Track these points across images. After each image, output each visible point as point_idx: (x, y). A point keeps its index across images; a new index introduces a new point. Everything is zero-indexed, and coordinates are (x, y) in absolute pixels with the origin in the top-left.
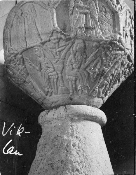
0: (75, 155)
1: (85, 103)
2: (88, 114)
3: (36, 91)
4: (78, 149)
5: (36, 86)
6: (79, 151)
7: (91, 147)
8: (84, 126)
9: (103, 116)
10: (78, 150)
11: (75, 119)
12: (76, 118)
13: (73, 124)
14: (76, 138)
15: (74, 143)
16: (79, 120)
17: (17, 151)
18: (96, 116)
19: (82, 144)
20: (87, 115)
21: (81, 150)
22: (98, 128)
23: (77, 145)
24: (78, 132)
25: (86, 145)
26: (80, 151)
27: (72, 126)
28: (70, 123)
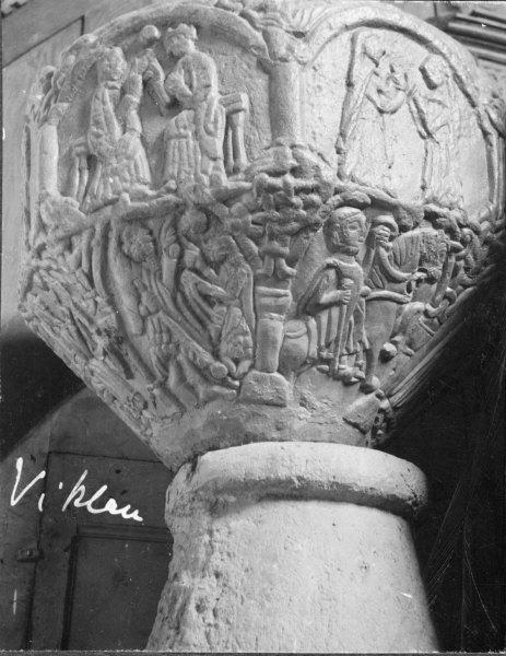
0: (195, 645)
1: (326, 436)
2: (259, 474)
3: (69, 309)
4: (211, 619)
5: (77, 48)
6: (213, 629)
7: (268, 605)
8: (259, 522)
9: (393, 473)
10: (209, 625)
11: (225, 505)
12: (232, 499)
13: (218, 524)
14: (217, 575)
15: (201, 601)
16: (240, 506)
17: (128, 507)
18: (300, 478)
19: (233, 597)
20: (256, 483)
21: (222, 624)
22: (386, 531)
23: (212, 604)
24: (229, 555)
25: (247, 602)
26: (216, 626)
27: (210, 533)
28: (205, 520)
